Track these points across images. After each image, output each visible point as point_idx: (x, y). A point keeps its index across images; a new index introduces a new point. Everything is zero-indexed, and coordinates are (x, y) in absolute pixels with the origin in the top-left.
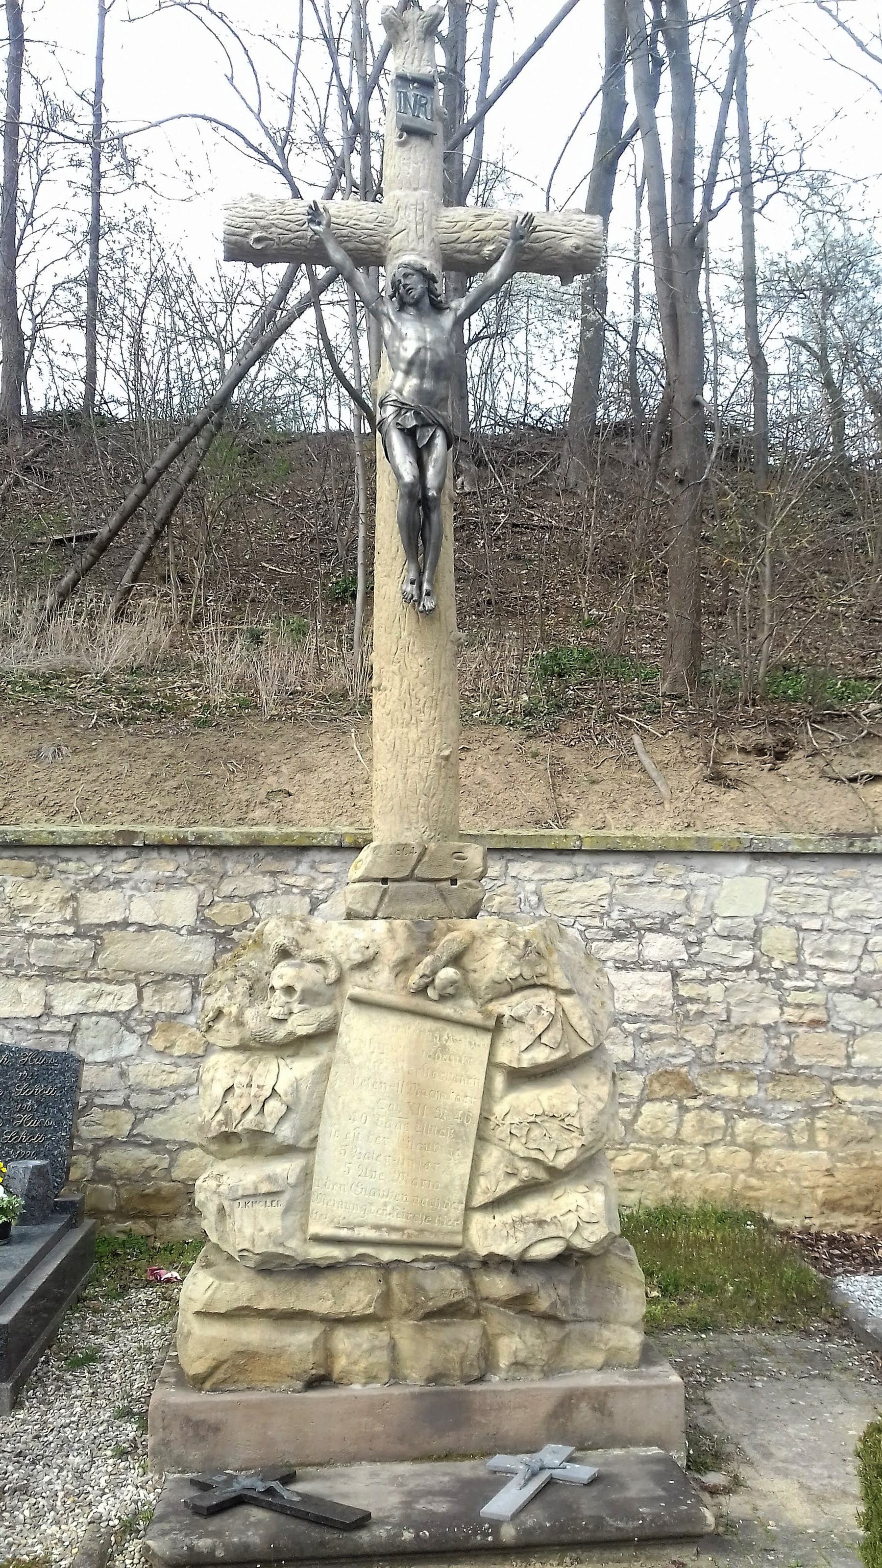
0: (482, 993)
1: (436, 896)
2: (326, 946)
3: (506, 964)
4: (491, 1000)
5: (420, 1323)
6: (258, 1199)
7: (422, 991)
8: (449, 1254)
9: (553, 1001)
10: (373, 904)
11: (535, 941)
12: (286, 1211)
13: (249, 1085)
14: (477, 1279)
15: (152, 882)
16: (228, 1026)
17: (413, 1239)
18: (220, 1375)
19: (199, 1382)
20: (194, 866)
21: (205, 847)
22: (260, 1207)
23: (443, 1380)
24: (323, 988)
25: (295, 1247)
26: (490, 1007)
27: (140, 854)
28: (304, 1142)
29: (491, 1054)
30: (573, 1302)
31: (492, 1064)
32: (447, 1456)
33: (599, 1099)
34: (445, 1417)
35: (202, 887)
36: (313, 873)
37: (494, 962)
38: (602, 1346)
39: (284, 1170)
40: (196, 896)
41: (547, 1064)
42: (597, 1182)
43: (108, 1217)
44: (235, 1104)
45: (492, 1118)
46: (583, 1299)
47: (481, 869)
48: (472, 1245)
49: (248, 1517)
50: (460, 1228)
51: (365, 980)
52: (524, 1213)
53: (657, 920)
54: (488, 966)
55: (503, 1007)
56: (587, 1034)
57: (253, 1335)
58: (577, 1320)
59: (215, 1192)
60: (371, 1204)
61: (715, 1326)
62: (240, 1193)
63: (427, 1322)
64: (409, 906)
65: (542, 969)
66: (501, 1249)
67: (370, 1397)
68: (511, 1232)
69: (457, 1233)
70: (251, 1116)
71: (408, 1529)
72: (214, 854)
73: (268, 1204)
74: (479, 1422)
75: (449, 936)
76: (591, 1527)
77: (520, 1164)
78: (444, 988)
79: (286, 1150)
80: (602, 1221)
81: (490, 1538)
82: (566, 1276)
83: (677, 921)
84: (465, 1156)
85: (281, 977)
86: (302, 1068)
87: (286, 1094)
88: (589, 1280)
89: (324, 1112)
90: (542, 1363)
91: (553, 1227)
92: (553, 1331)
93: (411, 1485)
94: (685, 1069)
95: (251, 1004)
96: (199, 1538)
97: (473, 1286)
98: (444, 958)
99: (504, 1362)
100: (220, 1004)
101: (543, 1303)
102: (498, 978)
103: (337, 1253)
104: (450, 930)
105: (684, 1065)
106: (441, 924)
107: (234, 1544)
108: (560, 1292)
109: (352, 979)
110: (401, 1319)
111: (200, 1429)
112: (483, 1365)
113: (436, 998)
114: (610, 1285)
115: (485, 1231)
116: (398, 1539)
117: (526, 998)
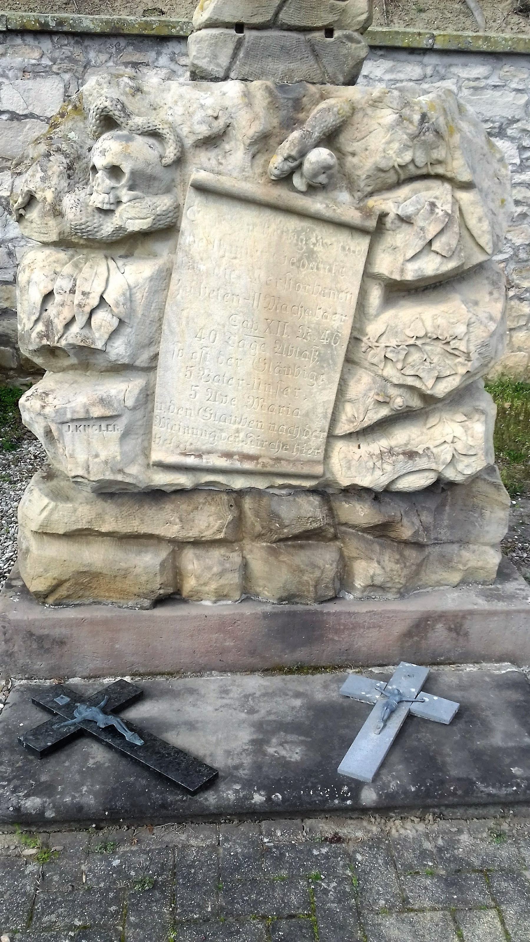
0: (362, 184)
1: (307, 53)
2: (163, 114)
3: (396, 146)
4: (371, 194)
5: (274, 545)
6: (91, 423)
7: (285, 179)
8: (308, 484)
9: (449, 198)
10: (224, 60)
11: (433, 115)
12: (125, 435)
13: (72, 291)
14: (336, 504)
15: (19, 69)
16: (43, 215)
17: (269, 469)
18: (63, 591)
19: (42, 597)
20: (57, 54)
21: (67, 34)
22: (93, 431)
23: (297, 600)
24: (158, 171)
25: (136, 474)
26: (371, 202)
27: (5, 40)
28: (142, 360)
29: (369, 261)
30: (435, 527)
31: (368, 275)
32: (300, 669)
33: (491, 318)
34: (297, 637)
35: (67, 76)
36: (173, 66)
37: (379, 142)
38: (461, 567)
39: (119, 392)
40: (62, 85)
41: (436, 276)
42: (477, 410)
43: (11, 373)
44: (58, 314)
45: (365, 339)
46: (446, 522)
47: (364, 17)
48: (333, 474)
49: (86, 756)
50: (321, 456)
51: (214, 162)
52: (393, 443)
53: (497, 125)
54: (372, 147)
55: (389, 203)
56: (485, 240)
57: (95, 556)
58: (438, 542)
59: (40, 414)
60: (222, 430)
61: (523, 492)
62: (69, 416)
63: (282, 544)
64: (271, 65)
65: (439, 154)
66: (366, 481)
67: (221, 617)
68: (378, 464)
69: (318, 462)
70: (75, 329)
71: (258, 791)
72: (77, 42)
73: (104, 428)
74: (332, 640)
75: (323, 105)
76: (459, 792)
77: (393, 392)
78: (315, 175)
79: (119, 369)
80: (480, 452)
81: (349, 802)
82: (432, 503)
83: (515, 126)
84: (330, 381)
85: (103, 153)
86: (132, 274)
87: (117, 304)
88: (453, 505)
89: (165, 327)
90: (399, 586)
91: (425, 459)
92: (412, 554)
93: (264, 709)
94: (502, 265)
95: (70, 189)
96: (27, 796)
97: (331, 512)
98: (316, 134)
99: (359, 583)
100: (31, 187)
101: (406, 532)
102: (383, 164)
103: (184, 480)
104: (323, 97)
105: (502, 261)
106: (313, 89)
107: (65, 804)
108: (423, 518)
109: (196, 160)
110: (253, 541)
111: (42, 642)
112: (338, 585)
113: (303, 188)
114: (474, 508)
115: (349, 462)
116: (247, 802)
117: (416, 192)
